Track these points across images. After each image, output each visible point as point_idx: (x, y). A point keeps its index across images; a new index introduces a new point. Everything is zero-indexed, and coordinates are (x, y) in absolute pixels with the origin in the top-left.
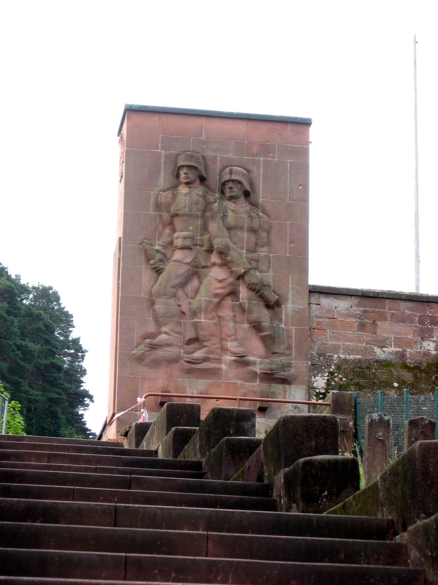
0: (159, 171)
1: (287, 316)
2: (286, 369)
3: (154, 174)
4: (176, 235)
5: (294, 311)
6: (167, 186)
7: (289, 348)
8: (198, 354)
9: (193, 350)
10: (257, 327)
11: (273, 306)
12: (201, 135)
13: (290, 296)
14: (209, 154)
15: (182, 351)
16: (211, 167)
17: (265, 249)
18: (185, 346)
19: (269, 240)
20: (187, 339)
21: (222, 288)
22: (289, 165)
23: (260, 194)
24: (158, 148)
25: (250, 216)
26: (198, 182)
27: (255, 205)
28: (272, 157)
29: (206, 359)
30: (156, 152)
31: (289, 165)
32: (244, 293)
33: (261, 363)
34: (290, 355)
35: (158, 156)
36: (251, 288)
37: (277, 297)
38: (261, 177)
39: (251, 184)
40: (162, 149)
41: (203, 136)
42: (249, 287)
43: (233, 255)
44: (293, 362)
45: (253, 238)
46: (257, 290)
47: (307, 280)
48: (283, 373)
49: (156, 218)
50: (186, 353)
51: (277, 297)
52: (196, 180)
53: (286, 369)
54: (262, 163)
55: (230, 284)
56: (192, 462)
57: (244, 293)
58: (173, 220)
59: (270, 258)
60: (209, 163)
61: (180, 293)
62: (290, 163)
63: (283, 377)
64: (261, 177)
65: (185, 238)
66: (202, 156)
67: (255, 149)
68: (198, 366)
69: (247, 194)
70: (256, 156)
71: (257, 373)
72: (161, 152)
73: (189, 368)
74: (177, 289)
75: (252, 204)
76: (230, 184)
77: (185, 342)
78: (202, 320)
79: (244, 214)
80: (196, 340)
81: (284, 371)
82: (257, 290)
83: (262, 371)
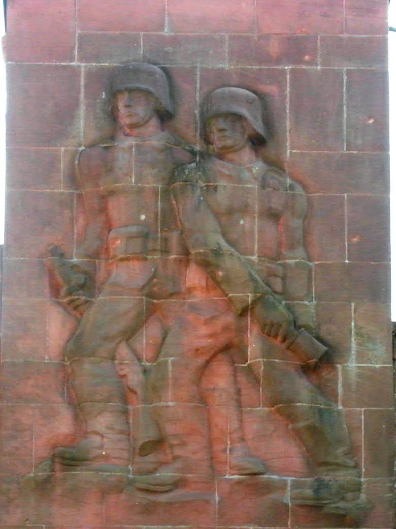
0: (75, 105)
1: (346, 386)
2: (350, 495)
3: (64, 115)
4: (112, 234)
5: (360, 376)
6: (93, 135)
7: (353, 451)
8: (166, 474)
9: (155, 466)
10: (283, 407)
11: (319, 363)
12: (162, 27)
13: (354, 345)
14: (179, 62)
15: (130, 467)
16: (183, 86)
17: (300, 252)
18: (138, 459)
19: (306, 232)
20: (140, 443)
21: (211, 336)
22: (345, 78)
23: (285, 142)
24: (72, 59)
25: (263, 186)
26: (154, 122)
27: (275, 165)
28: (307, 63)
29: (177, 484)
30: (68, 66)
31: (345, 78)
32: (254, 345)
33: (296, 485)
34: (357, 466)
35: (75, 72)
36: (269, 330)
37: (324, 348)
38: (288, 106)
39: (268, 122)
40: (81, 59)
41: (166, 30)
42: (266, 331)
43: (231, 264)
44: (362, 480)
45: (271, 230)
46: (285, 334)
47: (388, 312)
48: (341, 504)
49: (72, 201)
50: (140, 472)
51: (324, 348)
52: (150, 118)
53: (350, 495)
54: (288, 76)
55: (226, 328)
56: (338, 391)
57: (254, 345)
58: (106, 203)
59: (310, 271)
60: (178, 81)
61: (124, 351)
62: (349, 73)
63: (341, 512)
64: (288, 106)
65: (130, 237)
66: (164, 70)
67: (274, 48)
68: (163, 498)
69: (258, 142)
70: (278, 61)
71: (286, 505)
72: (79, 67)
73: (144, 502)
74: (118, 344)
75: (269, 162)
76: (221, 124)
77: (137, 450)
78: (171, 404)
79: (252, 183)
80: (158, 444)
81: (343, 499)
82: (285, 334)
83: (297, 502)
